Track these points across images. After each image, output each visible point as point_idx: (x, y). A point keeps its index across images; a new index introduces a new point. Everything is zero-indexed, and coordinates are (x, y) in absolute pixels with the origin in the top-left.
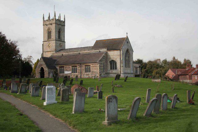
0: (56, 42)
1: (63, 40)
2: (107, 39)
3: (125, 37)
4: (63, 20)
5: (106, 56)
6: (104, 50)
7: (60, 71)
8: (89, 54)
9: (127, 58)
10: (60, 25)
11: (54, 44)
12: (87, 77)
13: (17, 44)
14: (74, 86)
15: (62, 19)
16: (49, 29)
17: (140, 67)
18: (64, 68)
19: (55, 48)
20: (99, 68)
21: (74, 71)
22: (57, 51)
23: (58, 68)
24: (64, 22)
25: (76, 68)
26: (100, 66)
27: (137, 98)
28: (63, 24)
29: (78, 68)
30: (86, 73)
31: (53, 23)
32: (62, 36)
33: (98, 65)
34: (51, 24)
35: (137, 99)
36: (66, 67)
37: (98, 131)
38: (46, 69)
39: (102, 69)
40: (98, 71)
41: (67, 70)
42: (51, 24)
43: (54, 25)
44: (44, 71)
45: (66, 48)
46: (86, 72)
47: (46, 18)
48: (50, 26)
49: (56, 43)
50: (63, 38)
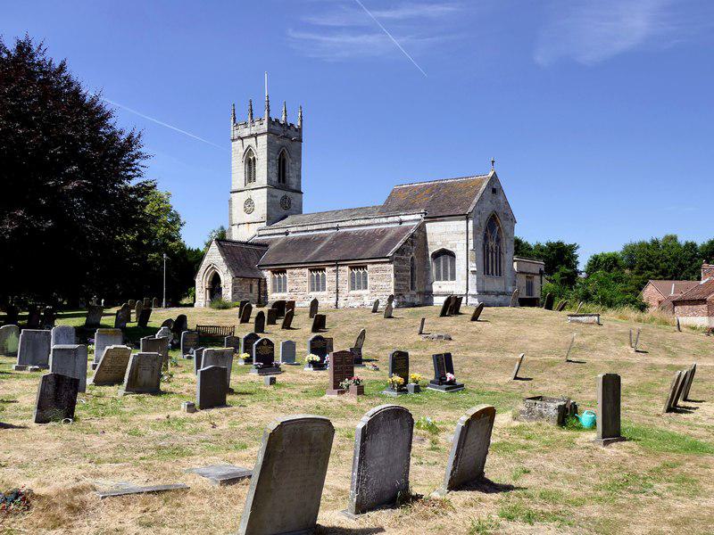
0: (268, 193)
1: (294, 187)
5: (418, 239)
7: (274, 286)
9: (492, 244)
11: (264, 200)
12: (357, 304)
14: (528, 334)
18: (287, 275)
19: (266, 212)
20: (395, 276)
22: (272, 219)
25: (324, 275)
26: (397, 271)
27: (484, 406)
30: (352, 292)
31: (262, 131)
32: (291, 175)
33: (392, 266)
34: (256, 136)
35: (468, 422)
36: (292, 273)
39: (404, 280)
40: (392, 284)
43: (263, 140)
44: (222, 285)
46: (353, 288)
48: (251, 141)
49: (269, 195)
50: (293, 180)
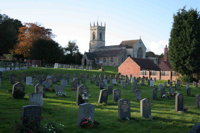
2: (131, 40)
3: (139, 39)
4: (104, 26)
6: (124, 48)
8: (115, 50)
10: (101, 31)
13: (76, 42)
15: (103, 26)
16: (94, 33)
17: (156, 60)
21: (105, 61)
23: (96, 59)
24: (105, 27)
28: (103, 29)
29: (107, 59)
32: (103, 38)
34: (95, 29)
37: (70, 132)
38: (87, 60)
41: (101, 61)
42: (95, 29)
45: (106, 46)
47: (92, 25)
